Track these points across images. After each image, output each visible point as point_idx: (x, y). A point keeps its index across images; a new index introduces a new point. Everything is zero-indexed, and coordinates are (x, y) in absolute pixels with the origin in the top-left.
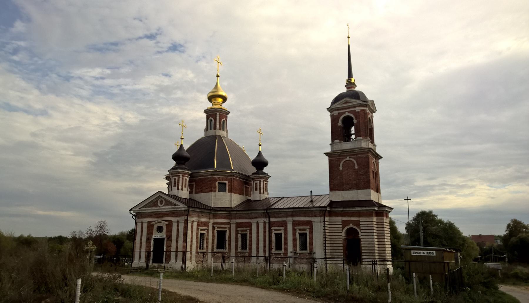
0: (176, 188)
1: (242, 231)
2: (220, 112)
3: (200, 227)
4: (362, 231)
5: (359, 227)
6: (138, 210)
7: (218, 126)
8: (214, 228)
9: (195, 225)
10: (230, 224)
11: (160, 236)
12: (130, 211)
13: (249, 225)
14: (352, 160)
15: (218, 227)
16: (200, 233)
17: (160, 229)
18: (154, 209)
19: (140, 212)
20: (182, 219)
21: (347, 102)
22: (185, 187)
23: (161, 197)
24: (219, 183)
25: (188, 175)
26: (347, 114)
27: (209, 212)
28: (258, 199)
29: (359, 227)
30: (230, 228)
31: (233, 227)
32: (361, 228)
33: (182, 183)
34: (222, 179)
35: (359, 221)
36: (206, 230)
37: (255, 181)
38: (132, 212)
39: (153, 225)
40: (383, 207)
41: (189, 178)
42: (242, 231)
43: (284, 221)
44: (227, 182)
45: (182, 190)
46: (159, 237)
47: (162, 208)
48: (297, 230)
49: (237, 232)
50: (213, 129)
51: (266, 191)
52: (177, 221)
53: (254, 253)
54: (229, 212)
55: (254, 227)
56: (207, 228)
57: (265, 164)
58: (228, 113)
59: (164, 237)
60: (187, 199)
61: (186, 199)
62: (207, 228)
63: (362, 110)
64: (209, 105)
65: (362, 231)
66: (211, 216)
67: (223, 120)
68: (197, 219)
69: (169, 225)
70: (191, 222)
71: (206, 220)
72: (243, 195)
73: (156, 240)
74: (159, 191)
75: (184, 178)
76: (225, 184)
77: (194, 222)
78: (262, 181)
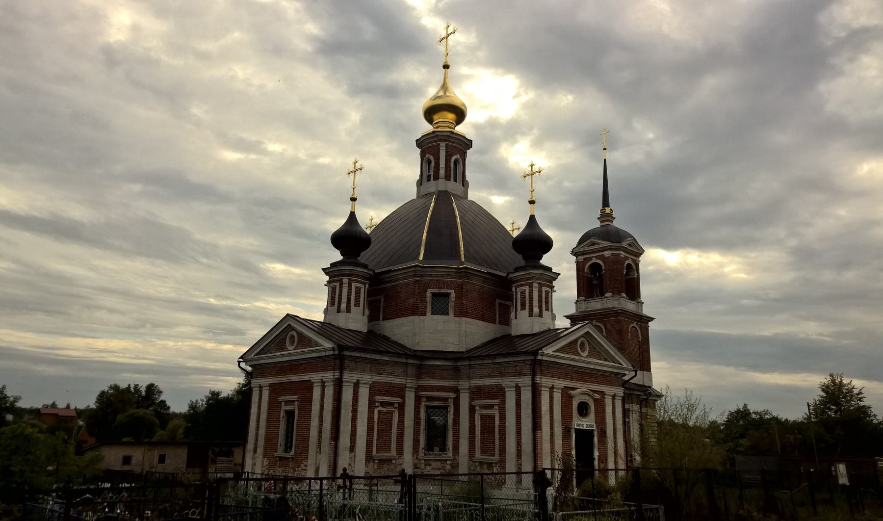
1: (483, 407)
2: (447, 141)
3: (379, 398)
6: (551, 356)
7: (442, 172)
8: (418, 399)
9: (364, 392)
10: (456, 390)
11: (587, 426)
12: (239, 362)
13: (499, 393)
17: (583, 409)
18: (279, 357)
19: (555, 360)
20: (329, 376)
22: (357, 304)
23: (293, 329)
24: (434, 295)
27: (405, 361)
28: (536, 330)
31: (465, 400)
37: (521, 286)
38: (243, 365)
41: (367, 286)
42: (483, 407)
43: (497, 386)
44: (452, 292)
45: (348, 310)
46: (585, 428)
47: (291, 352)
49: (472, 409)
51: (547, 309)
53: (510, 466)
56: (399, 399)
59: (594, 429)
60: (360, 332)
61: (357, 331)
62: (399, 400)
64: (428, 128)
66: (411, 370)
67: (453, 159)
68: (367, 378)
70: (548, 390)
71: (399, 381)
72: (494, 322)
75: (354, 285)
76: (448, 295)
77: (554, 390)
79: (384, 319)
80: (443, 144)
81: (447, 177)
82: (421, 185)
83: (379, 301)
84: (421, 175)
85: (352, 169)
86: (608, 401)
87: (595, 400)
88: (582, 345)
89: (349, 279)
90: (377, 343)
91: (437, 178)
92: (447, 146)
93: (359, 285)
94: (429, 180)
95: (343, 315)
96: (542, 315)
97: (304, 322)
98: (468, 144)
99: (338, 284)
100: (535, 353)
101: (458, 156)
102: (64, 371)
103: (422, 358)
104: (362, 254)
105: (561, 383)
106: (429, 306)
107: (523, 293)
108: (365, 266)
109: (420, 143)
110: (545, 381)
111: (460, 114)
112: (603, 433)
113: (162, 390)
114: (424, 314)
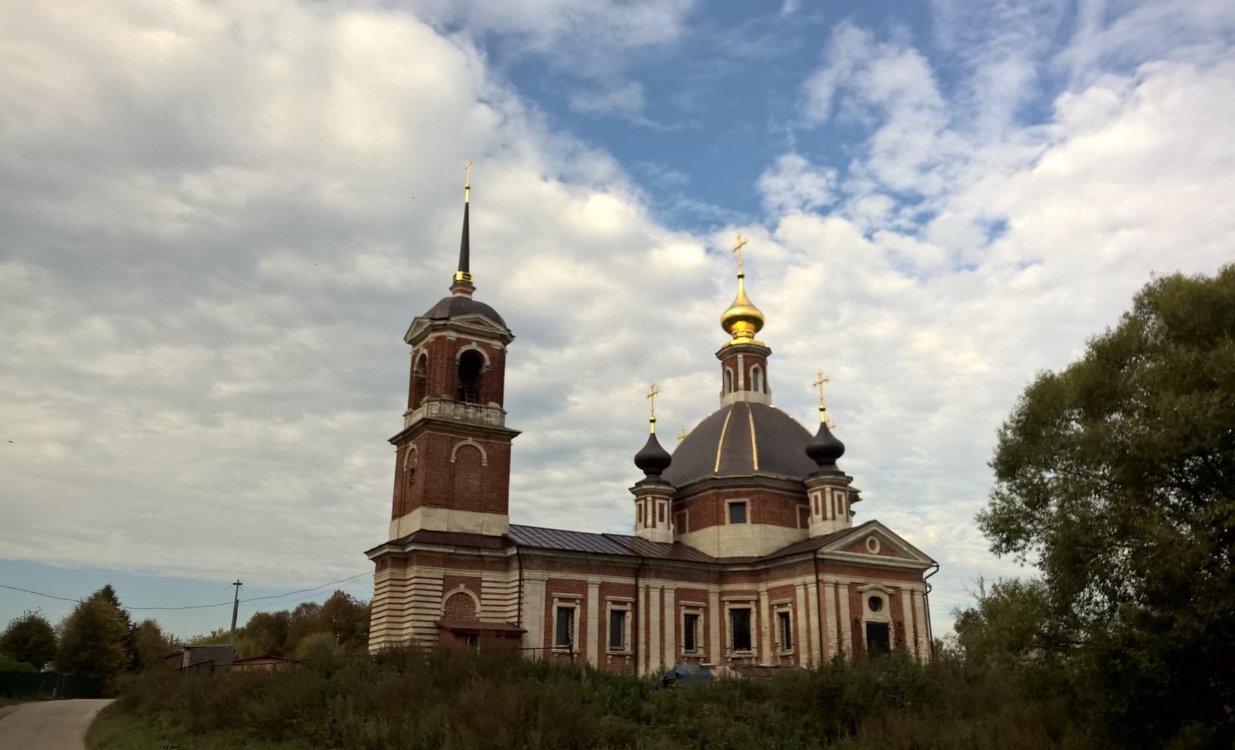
0: (820, 516)
4: (484, 602)
5: (479, 593)
8: (722, 603)
9: (670, 597)
10: (758, 593)
13: (791, 590)
14: (480, 448)
15: (561, 599)
16: (686, 615)
21: (477, 322)
24: (731, 505)
25: (668, 495)
26: (474, 346)
29: (479, 593)
30: (758, 602)
32: (483, 596)
33: (654, 512)
34: (737, 495)
35: (480, 580)
36: (790, 605)
39: (861, 593)
40: (854, 531)
41: (671, 501)
45: (654, 526)
48: (556, 600)
50: (733, 390)
52: (645, 588)
54: (758, 568)
55: (800, 592)
57: (837, 450)
58: (767, 352)
63: (438, 338)
65: (484, 602)
68: (671, 585)
69: (895, 597)
72: (795, 526)
73: (870, 625)
74: (875, 521)
75: (658, 502)
76: (743, 504)
78: (649, 499)
79: (691, 531)
80: (740, 356)
81: (747, 387)
82: (724, 396)
83: (684, 515)
84: (724, 387)
85: (651, 393)
86: (906, 599)
87: (890, 595)
88: (872, 542)
89: (653, 497)
90: (662, 552)
91: (736, 389)
92: (745, 357)
93: (662, 502)
94: (730, 392)
95: (649, 530)
96: (755, 523)
97: (612, 537)
98: (767, 352)
99: (642, 502)
100: (815, 552)
101: (757, 365)
102: (744, 346)
103: (724, 565)
104: (664, 471)
105: (846, 579)
106: (727, 516)
107: (816, 498)
108: (667, 484)
109: (720, 355)
110: (829, 578)
111: (756, 323)
112: (900, 626)
113: (476, 287)
114: (723, 523)
